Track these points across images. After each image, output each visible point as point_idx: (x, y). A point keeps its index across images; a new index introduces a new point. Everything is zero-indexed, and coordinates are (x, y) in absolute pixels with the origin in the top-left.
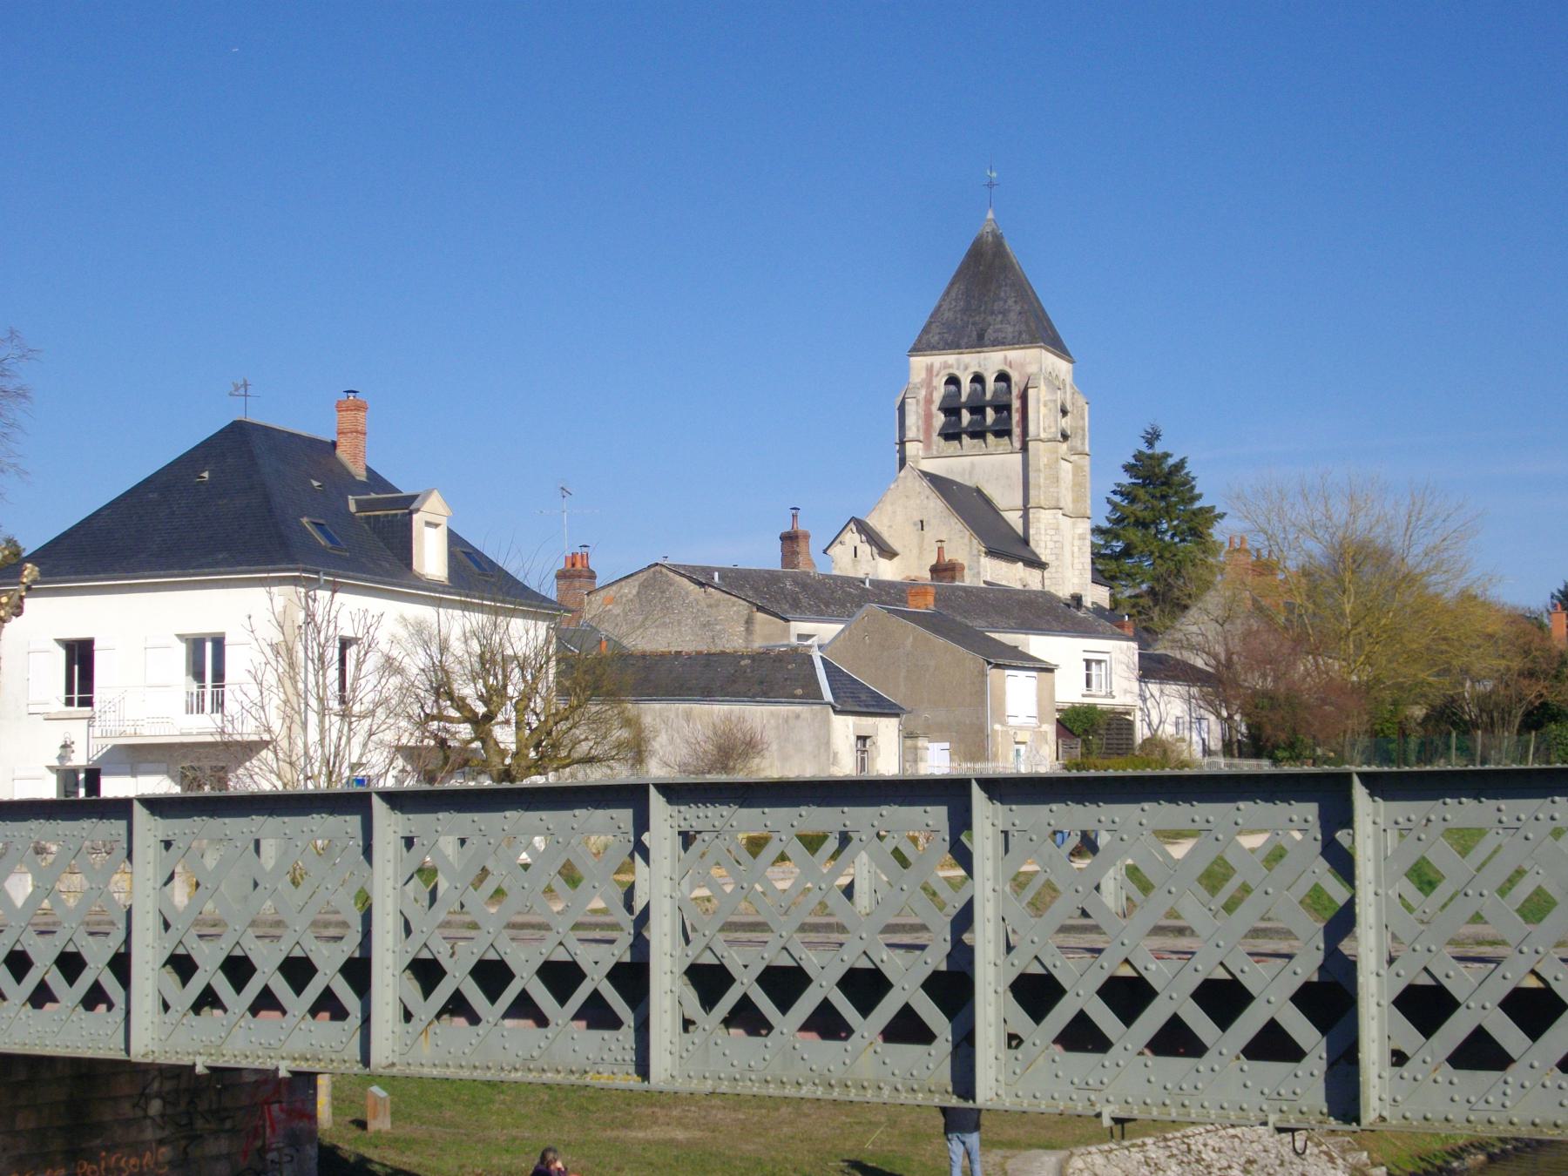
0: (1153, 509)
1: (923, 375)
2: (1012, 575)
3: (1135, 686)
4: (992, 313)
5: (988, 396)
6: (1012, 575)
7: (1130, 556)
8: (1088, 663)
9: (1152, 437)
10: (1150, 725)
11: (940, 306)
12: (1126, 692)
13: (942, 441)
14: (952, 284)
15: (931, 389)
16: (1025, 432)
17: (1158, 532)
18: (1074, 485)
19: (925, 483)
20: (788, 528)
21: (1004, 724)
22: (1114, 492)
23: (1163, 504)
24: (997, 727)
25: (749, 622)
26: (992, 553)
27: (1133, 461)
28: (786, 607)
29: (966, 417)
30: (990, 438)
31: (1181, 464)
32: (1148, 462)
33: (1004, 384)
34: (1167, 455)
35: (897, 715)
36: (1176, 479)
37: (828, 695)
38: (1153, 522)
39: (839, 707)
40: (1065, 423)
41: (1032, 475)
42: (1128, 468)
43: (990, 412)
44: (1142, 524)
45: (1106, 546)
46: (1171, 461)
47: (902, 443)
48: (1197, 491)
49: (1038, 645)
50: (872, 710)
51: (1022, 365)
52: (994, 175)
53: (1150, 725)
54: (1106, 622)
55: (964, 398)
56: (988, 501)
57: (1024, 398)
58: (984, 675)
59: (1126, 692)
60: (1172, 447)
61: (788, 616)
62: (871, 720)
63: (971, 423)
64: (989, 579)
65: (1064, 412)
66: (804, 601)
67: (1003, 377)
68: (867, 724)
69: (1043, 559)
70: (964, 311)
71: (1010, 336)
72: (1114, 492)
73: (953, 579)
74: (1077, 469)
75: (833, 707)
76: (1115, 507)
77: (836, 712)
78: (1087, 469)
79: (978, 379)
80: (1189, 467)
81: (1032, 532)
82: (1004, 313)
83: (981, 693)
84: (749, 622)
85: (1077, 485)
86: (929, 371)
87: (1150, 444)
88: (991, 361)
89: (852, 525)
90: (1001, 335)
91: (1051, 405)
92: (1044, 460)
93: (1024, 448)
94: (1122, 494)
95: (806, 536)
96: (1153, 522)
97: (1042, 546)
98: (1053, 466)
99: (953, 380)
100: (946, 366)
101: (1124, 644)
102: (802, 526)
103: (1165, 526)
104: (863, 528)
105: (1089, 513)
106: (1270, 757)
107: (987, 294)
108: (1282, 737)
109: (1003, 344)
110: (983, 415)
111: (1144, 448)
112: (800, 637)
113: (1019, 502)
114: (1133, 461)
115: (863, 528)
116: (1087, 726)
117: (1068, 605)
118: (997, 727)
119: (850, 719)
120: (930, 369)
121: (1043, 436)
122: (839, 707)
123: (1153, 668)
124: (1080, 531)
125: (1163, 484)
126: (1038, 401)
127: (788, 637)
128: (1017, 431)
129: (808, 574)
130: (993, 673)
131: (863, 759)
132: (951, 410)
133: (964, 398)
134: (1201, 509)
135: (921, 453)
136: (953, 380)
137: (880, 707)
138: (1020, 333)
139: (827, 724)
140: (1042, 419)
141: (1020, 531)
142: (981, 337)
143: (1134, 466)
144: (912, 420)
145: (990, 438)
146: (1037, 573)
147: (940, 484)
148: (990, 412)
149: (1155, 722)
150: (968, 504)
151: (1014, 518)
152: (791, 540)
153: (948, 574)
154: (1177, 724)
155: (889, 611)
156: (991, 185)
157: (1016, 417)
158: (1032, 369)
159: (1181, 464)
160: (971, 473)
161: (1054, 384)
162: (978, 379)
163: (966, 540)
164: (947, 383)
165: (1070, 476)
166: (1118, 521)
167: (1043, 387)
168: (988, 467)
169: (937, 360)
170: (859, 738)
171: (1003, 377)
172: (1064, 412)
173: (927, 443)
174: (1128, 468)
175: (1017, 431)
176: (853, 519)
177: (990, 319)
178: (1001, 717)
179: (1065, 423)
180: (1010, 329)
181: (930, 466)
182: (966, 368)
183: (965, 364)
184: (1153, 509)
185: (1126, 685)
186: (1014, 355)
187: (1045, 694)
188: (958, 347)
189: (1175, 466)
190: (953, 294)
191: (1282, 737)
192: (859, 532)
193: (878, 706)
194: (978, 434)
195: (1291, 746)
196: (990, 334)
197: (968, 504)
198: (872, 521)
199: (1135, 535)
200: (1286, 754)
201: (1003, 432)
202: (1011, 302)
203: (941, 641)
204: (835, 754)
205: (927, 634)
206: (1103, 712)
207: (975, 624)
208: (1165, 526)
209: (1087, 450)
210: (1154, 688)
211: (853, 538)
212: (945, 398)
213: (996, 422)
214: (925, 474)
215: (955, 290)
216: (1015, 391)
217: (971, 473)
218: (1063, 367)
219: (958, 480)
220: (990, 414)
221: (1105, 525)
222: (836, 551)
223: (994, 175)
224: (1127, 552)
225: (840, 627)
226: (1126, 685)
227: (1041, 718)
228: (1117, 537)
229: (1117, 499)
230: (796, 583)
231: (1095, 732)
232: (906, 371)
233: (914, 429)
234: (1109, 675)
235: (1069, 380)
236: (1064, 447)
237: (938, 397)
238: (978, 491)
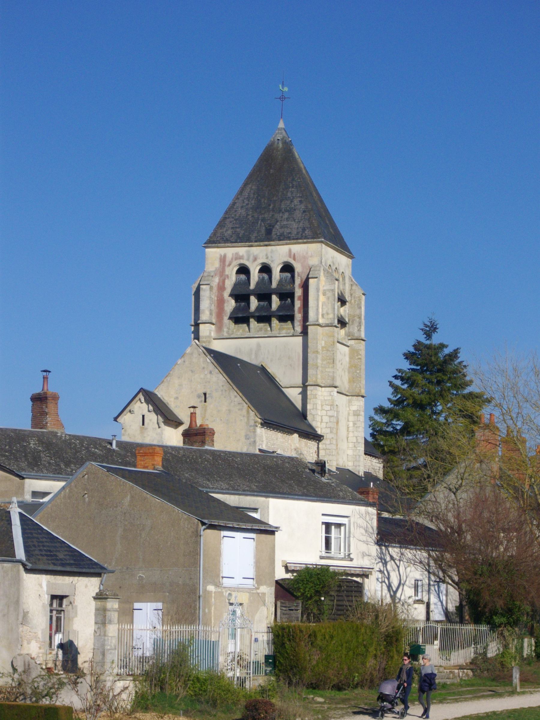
0: (429, 393)
1: (217, 264)
2: (287, 445)
3: (374, 549)
4: (280, 211)
5: (274, 285)
6: (287, 445)
7: (409, 433)
8: (328, 526)
9: (430, 330)
10: (389, 587)
11: (234, 204)
12: (364, 555)
13: (232, 325)
14: (245, 184)
15: (223, 277)
16: (305, 318)
17: (434, 413)
18: (351, 367)
19: (209, 359)
20: (38, 390)
21: (218, 585)
22: (396, 377)
23: (438, 389)
24: (211, 588)
26: (267, 424)
27: (412, 350)
28: (24, 465)
29: (254, 303)
30: (275, 322)
31: (454, 355)
32: (425, 351)
33: (289, 275)
34: (442, 346)
35: (98, 575)
36: (450, 367)
37: (20, 553)
38: (430, 404)
39: (29, 566)
40: (344, 311)
41: (310, 356)
42: (408, 356)
43: (275, 300)
44: (419, 406)
45: (388, 424)
46: (447, 351)
47: (197, 325)
48: (468, 378)
49: (277, 510)
50: (68, 569)
51: (305, 258)
52: (286, 89)
53: (389, 587)
54: (353, 488)
55: (252, 286)
56: (271, 379)
57: (305, 287)
58: (198, 535)
59: (364, 555)
60: (446, 338)
61: (23, 473)
62: (67, 580)
63: (258, 309)
64: (264, 448)
65: (342, 301)
66: (45, 458)
67: (288, 268)
68: (63, 583)
69: (319, 432)
70: (257, 208)
71: (295, 232)
72: (396, 377)
73: (203, 443)
74: (354, 353)
75: (24, 565)
76: (396, 389)
77: (28, 571)
78: (363, 353)
79: (266, 269)
80: (462, 357)
81: (309, 407)
82: (291, 211)
83: (194, 555)
85: (353, 367)
86: (222, 261)
87: (429, 336)
88: (277, 254)
89: (141, 396)
90: (287, 231)
91: (329, 294)
92: (322, 343)
93: (305, 332)
94: (402, 379)
95: (55, 398)
96: (430, 404)
97: (318, 420)
98: (330, 349)
99: (243, 270)
100: (237, 257)
101: (363, 509)
102: (52, 389)
103: (440, 408)
104: (151, 399)
105: (363, 392)
106: (488, 623)
107: (277, 196)
108: (500, 603)
109: (289, 238)
110: (269, 301)
111: (422, 338)
112: (35, 494)
113: (299, 380)
114: (412, 350)
115: (151, 399)
116: (318, 588)
117: (313, 471)
118: (211, 588)
119: (44, 579)
120: (223, 260)
121: (321, 321)
122: (29, 566)
123: (389, 534)
124: (354, 408)
125: (439, 371)
126: (318, 290)
127: (22, 494)
128: (298, 316)
129: (55, 434)
130: (208, 535)
131: (59, 619)
132: (241, 296)
133: (252, 286)
134: (471, 394)
135: (213, 334)
136: (243, 270)
137: (81, 566)
138: (304, 230)
139: (17, 582)
140: (321, 306)
141: (299, 405)
142: (269, 232)
143: (413, 354)
144: (205, 304)
145: (275, 322)
146: (312, 444)
147: (225, 362)
148: (275, 300)
149: (395, 583)
150: (252, 383)
151: (294, 395)
152: (40, 400)
153: (199, 438)
154: (416, 587)
155: (109, 469)
156: (282, 98)
157: (298, 304)
158: (313, 261)
159: (454, 355)
160: (256, 355)
161: (333, 274)
162: (266, 269)
163: (244, 412)
164: (239, 272)
165: (347, 359)
166: (398, 402)
167: (322, 278)
168: (271, 348)
169: (230, 252)
170: (53, 597)
171: (288, 268)
172: (342, 301)
173: (219, 326)
174: (408, 356)
175: (298, 316)
176: (142, 390)
177: (278, 216)
178: (215, 577)
179: (344, 311)
180: (295, 225)
181: (219, 346)
182: (255, 259)
183: (255, 255)
184: (429, 393)
185: (364, 548)
186: (298, 248)
187: (264, 560)
188: (248, 240)
189: (450, 355)
190: (246, 194)
191: (500, 603)
192: (147, 402)
193: (77, 565)
194: (264, 318)
195: (509, 611)
196: (277, 230)
197: (252, 383)
198: (161, 393)
199: (412, 415)
200: (504, 620)
201: (286, 317)
202: (296, 201)
203: (156, 501)
204: (26, 614)
206: (335, 574)
207: (200, 486)
208: (440, 408)
209: (363, 336)
210: (394, 551)
211: (141, 407)
212: (237, 285)
213: (280, 308)
214: (210, 352)
215: (248, 189)
216: (298, 281)
217: (256, 355)
218: (343, 262)
219: (246, 359)
220: (275, 301)
221: (387, 405)
222: (126, 418)
223: (286, 89)
224: (406, 430)
225: (62, 484)
226: (364, 548)
227: (259, 579)
228: (397, 416)
229: (398, 382)
230: (41, 441)
231: (327, 594)
232: (202, 260)
233: (207, 312)
234: (347, 538)
235: (348, 272)
236: (343, 332)
237: (229, 284)
238: (263, 369)
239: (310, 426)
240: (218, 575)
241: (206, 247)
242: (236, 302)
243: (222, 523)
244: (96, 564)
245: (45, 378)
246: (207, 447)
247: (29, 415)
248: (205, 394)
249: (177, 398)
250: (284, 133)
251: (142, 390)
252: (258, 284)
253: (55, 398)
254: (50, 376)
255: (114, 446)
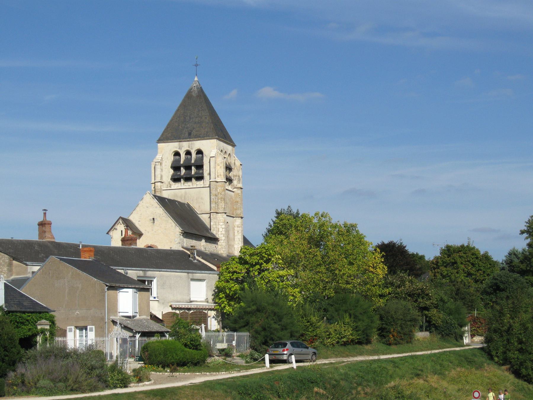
25: (10, 265)
30: (193, 180)
79: (188, 153)
84: (10, 265)
86: (166, 152)
89: (121, 221)
95: (50, 224)
99: (177, 154)
102: (48, 219)
107: (196, 117)
109: (200, 137)
110: (188, 169)
132: (176, 167)
136: (177, 154)
138: (207, 132)
142: (190, 134)
155: (61, 259)
162: (188, 153)
169: (173, 146)
183: (183, 146)
188: (179, 139)
194: (188, 179)
196: (194, 133)
201: (200, 178)
205: (79, 271)
212: (174, 162)
213: (196, 173)
219: (179, 200)
239: (212, 234)
240: (117, 311)
241: (158, 143)
242: (174, 171)
243: (117, 285)
244: (45, 308)
245: (45, 214)
246: (133, 246)
247: (37, 232)
248: (154, 219)
249: (139, 221)
250: (197, 83)
251: (121, 218)
252: (185, 161)
253: (50, 224)
254: (47, 212)
255: (81, 247)
